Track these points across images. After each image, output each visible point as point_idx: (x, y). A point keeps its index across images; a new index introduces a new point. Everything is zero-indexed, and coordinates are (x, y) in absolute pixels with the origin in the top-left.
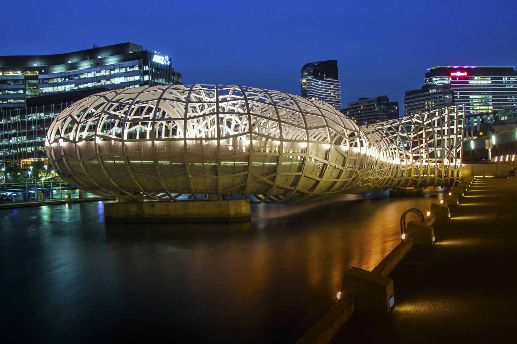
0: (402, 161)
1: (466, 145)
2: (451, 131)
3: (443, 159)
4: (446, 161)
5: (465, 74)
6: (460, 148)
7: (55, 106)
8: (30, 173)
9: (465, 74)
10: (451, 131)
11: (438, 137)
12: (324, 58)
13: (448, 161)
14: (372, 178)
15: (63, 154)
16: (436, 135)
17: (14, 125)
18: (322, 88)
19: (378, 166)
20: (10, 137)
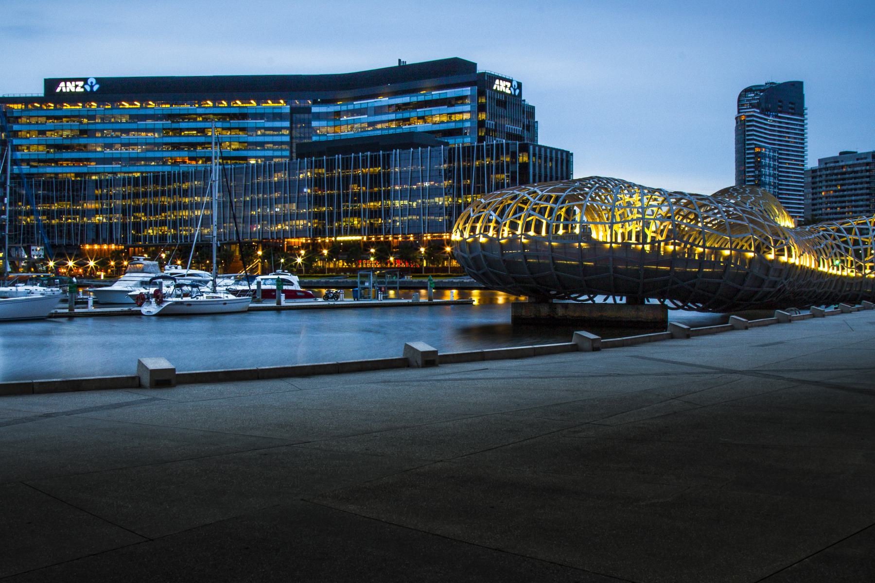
7: (343, 159)
8: (299, 260)
14: (806, 290)
17: (278, 186)
18: (774, 131)
19: (815, 276)
20: (272, 203)
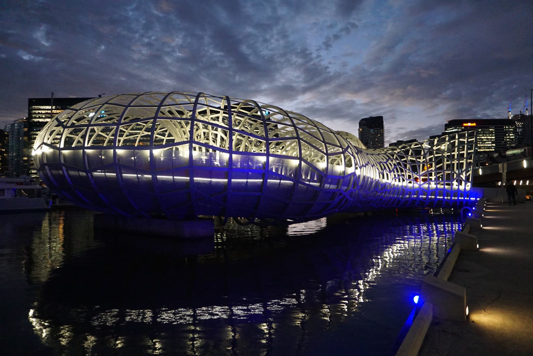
0: (410, 182)
1: (475, 172)
2: (461, 156)
3: (452, 182)
4: (455, 183)
5: (474, 124)
6: (470, 172)
9: (474, 124)
10: (461, 156)
11: (447, 161)
12: (374, 114)
13: (457, 184)
15: (62, 161)
16: (445, 159)
